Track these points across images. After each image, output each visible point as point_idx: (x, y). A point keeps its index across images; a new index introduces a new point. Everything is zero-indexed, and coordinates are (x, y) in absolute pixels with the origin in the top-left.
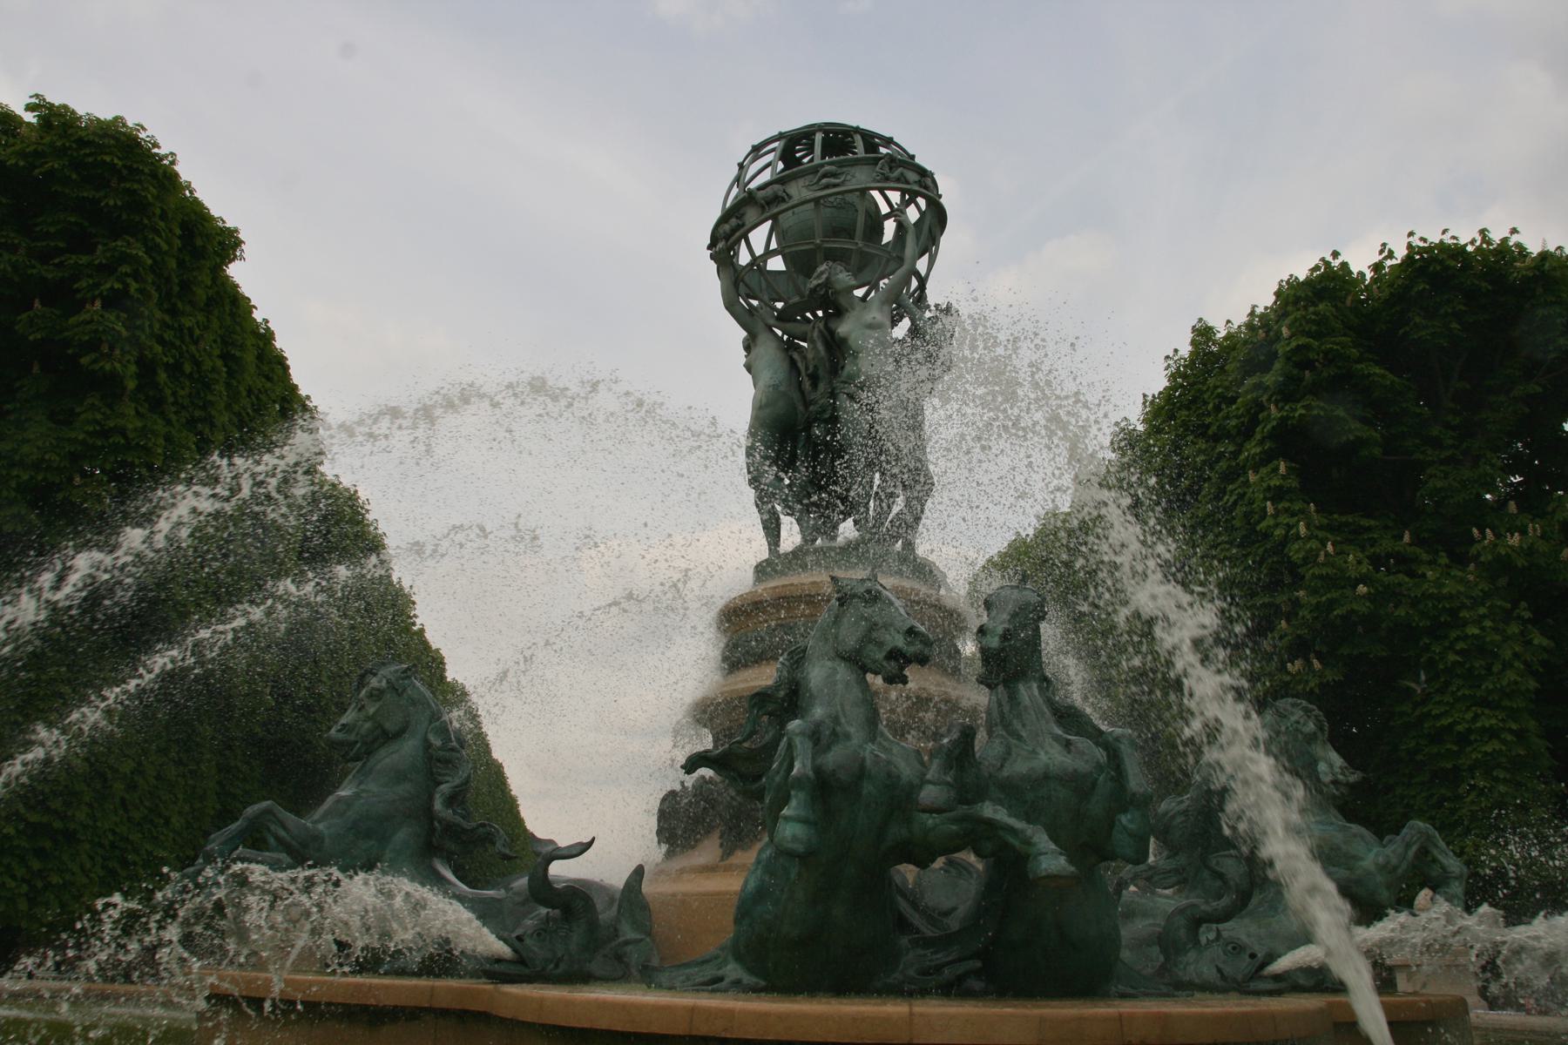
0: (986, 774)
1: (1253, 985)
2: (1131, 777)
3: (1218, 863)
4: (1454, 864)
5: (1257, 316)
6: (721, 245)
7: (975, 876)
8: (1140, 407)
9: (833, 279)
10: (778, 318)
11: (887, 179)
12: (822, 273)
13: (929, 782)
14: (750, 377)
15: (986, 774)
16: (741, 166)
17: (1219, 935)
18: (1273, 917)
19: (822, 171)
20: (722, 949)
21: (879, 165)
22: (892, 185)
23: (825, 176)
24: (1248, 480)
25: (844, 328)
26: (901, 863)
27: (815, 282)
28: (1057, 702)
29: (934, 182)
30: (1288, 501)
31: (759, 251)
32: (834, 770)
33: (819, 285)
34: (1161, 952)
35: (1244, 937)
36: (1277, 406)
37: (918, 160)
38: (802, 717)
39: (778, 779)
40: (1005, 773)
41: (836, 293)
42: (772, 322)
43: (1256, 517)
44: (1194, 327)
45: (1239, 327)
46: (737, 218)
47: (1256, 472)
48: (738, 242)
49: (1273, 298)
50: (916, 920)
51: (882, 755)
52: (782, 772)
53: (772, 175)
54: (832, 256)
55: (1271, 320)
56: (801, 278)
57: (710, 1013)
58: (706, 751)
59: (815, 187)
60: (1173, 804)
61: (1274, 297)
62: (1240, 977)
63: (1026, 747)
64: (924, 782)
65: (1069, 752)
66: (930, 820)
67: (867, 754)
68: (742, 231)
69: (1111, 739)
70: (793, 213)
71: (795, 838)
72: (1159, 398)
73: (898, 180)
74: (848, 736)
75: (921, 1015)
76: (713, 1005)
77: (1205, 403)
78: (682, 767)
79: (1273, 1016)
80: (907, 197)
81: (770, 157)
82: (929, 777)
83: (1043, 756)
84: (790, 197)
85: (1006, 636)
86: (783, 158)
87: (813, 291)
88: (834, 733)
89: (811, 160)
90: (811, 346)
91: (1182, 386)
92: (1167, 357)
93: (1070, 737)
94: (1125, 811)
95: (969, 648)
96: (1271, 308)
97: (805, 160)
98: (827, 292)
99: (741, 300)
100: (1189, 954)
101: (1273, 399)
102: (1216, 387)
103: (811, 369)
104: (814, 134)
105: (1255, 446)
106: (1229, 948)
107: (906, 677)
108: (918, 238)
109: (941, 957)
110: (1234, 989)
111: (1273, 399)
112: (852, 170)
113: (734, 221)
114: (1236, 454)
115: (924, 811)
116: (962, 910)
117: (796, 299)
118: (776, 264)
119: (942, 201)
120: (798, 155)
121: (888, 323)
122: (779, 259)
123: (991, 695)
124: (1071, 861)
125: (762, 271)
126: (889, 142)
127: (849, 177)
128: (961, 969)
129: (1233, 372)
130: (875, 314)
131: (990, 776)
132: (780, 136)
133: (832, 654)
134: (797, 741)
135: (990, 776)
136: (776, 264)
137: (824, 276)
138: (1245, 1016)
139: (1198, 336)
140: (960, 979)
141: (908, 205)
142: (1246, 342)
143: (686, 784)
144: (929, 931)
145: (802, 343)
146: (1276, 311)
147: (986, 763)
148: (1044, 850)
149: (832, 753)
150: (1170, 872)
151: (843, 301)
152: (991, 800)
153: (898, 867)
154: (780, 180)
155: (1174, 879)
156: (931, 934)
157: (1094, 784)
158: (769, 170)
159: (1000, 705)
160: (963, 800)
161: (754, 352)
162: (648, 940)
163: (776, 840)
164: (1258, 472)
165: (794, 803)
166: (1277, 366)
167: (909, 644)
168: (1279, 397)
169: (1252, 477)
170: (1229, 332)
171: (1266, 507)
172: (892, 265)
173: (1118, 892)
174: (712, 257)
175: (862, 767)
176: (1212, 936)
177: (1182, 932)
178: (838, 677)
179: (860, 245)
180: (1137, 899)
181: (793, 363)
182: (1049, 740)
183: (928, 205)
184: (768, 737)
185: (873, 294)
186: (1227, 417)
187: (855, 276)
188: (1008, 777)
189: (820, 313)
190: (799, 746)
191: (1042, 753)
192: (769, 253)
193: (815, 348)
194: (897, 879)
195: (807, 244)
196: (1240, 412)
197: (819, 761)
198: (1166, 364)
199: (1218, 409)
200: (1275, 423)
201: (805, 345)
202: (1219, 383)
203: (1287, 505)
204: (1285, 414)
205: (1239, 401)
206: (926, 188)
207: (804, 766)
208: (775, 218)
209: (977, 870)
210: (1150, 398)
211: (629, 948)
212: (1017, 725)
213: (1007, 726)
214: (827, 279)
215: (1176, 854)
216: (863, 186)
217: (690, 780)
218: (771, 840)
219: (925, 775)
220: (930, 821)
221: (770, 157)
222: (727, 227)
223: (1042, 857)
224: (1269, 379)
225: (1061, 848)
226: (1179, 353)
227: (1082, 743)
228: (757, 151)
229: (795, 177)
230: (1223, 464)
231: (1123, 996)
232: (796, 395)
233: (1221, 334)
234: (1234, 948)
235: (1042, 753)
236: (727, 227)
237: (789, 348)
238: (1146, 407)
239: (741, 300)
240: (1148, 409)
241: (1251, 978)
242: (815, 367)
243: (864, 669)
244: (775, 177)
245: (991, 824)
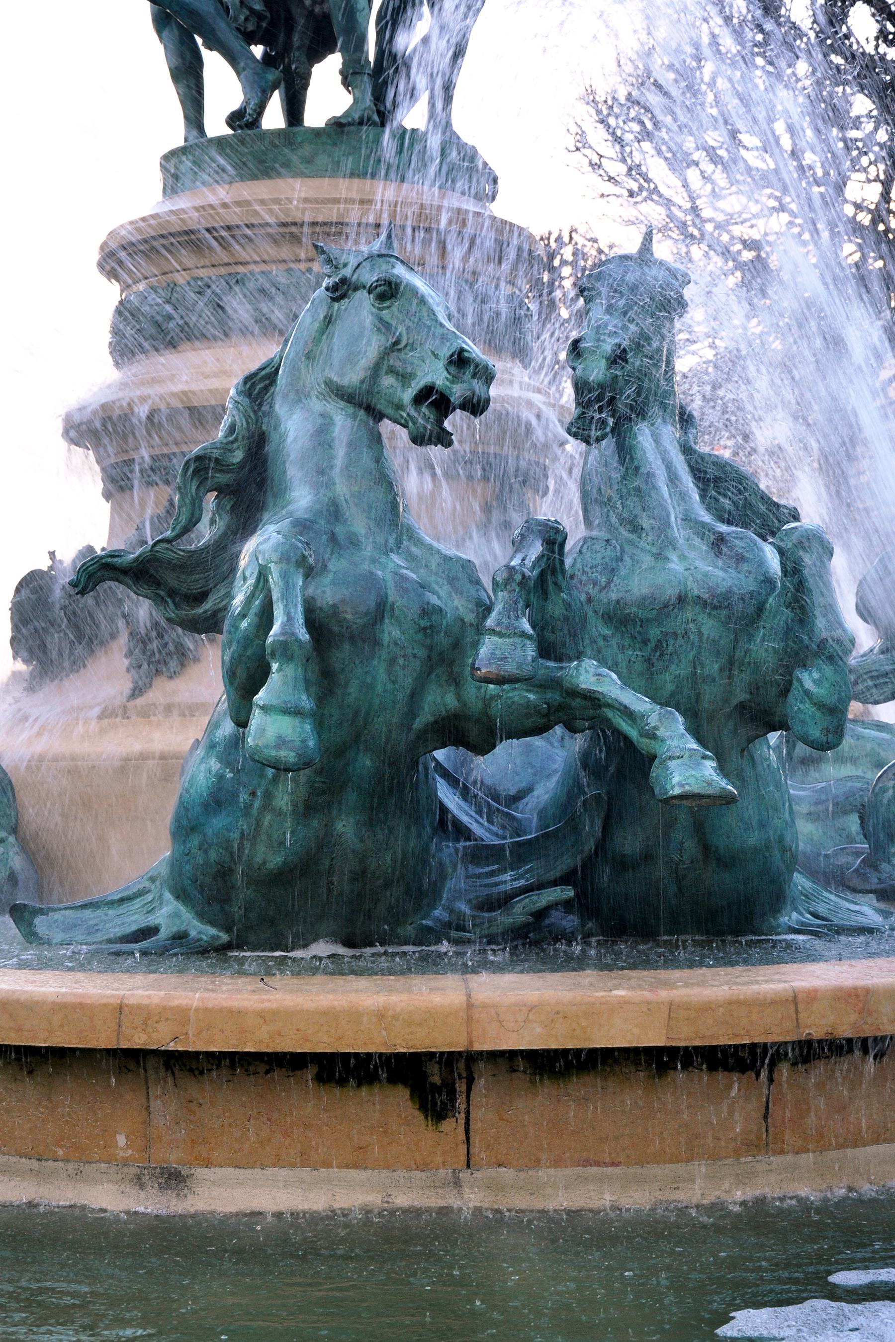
65: (719, 553)
71: (281, 742)
83: (675, 565)
109: (508, 880)
124: (722, 769)
131: (589, 600)
143: (58, 556)
165: (275, 678)
167: (455, 379)
188: (618, 602)
191: (674, 558)
197: (310, 591)
223: (672, 764)
235: (674, 558)
243: (379, 416)
245: (593, 700)
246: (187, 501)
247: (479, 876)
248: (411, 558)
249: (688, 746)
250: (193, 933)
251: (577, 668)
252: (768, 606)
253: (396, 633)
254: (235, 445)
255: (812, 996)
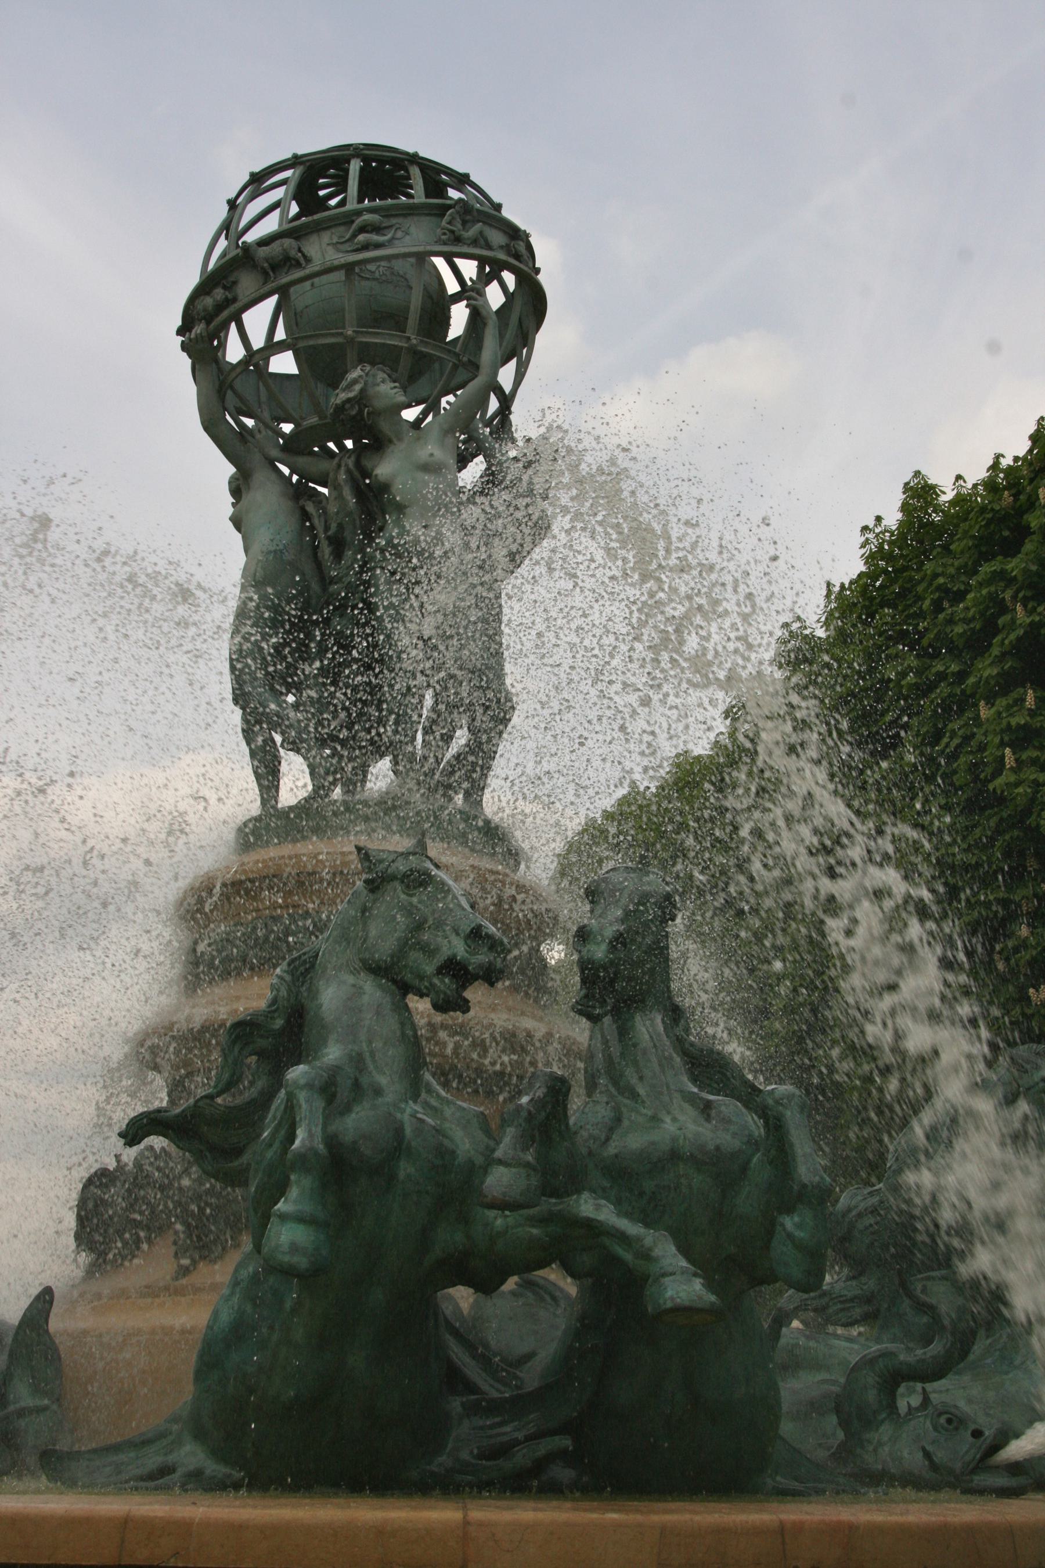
0: (584, 1151)
1: (981, 1479)
2: (800, 1159)
3: (924, 1290)
4: (996, 1001)
5: (1002, 471)
6: (198, 329)
7: (562, 1304)
8: (822, 602)
9: (371, 391)
10: (285, 449)
11: (458, 240)
12: (355, 382)
13: (500, 1162)
14: (239, 536)
15: (584, 1151)
16: (232, 204)
17: (926, 1400)
18: (1007, 1373)
19: (359, 221)
20: (175, 1419)
21: (447, 218)
22: (465, 249)
23: (362, 229)
24: (978, 715)
25: (384, 469)
26: (454, 1285)
27: (343, 396)
28: (692, 1044)
29: (530, 248)
30: (1035, 747)
31: (258, 342)
32: (355, 1142)
33: (349, 400)
34: (840, 1424)
35: (962, 1404)
36: (1025, 606)
37: (506, 213)
38: (309, 1063)
39: (269, 1154)
40: (612, 1149)
41: (375, 413)
42: (275, 453)
43: (989, 770)
44: (907, 484)
45: (975, 486)
46: (225, 288)
47: (990, 703)
48: (225, 327)
49: (1028, 444)
50: (472, 1370)
51: (429, 1120)
52: (277, 1145)
53: (280, 224)
54: (368, 355)
55: (1023, 477)
56: (320, 389)
57: (151, 1528)
58: (159, 1111)
59: (347, 247)
60: (860, 1198)
61: (1029, 443)
62: (958, 1466)
63: (645, 1111)
64: (490, 1162)
65: (708, 1119)
66: (499, 1221)
67: (406, 1118)
68: (232, 308)
69: (770, 1102)
70: (312, 285)
71: (294, 1248)
72: (850, 589)
73: (475, 242)
74: (378, 1092)
75: (481, 1524)
76: (160, 1514)
77: (919, 598)
78: (121, 1135)
79: (1010, 1532)
80: (488, 269)
81: (278, 193)
82: (498, 1154)
83: (669, 1126)
84: (308, 260)
85: (619, 941)
86: (298, 197)
87: (340, 409)
88: (357, 1085)
89: (342, 203)
90: (335, 494)
91: (885, 571)
92: (865, 529)
93: (711, 1097)
94: (789, 1210)
95: (555, 953)
96: (1024, 458)
97: (333, 202)
98: (361, 412)
99: (228, 417)
100: (882, 1429)
101: (1021, 595)
102: (936, 576)
103: (334, 527)
104: (349, 163)
105: (990, 665)
106: (942, 1420)
107: (467, 1001)
108: (501, 336)
109: (510, 1431)
110: (953, 1486)
111: (1021, 595)
112: (406, 222)
113: (219, 293)
114: (961, 676)
115: (492, 1206)
116: (547, 1353)
117: (314, 420)
118: (284, 364)
119: (541, 278)
120: (321, 193)
121: (452, 462)
122: (289, 355)
123: (592, 1031)
124: (709, 1285)
125: (262, 371)
126: (462, 180)
127: (399, 234)
128: (544, 1447)
129: (962, 552)
130: (432, 449)
131: (590, 1153)
132: (295, 161)
133: (358, 965)
134: (302, 1096)
135: (590, 1153)
136: (284, 364)
137: (357, 387)
138: (970, 1531)
139: (912, 498)
140: (539, 1467)
141: (488, 283)
142: (983, 509)
144: (493, 1391)
145: (320, 489)
146: (1031, 464)
147: (585, 1134)
148: (670, 1269)
149: (353, 1115)
150: (852, 1300)
151: (385, 426)
152: (593, 1191)
153: (451, 1291)
154: (291, 232)
155: (858, 1312)
156: (495, 1394)
157: (744, 1168)
158: (276, 213)
159: (606, 1042)
160: (549, 1190)
161: (246, 499)
162: (55, 1407)
163: (265, 1250)
164: (993, 705)
165: (294, 1192)
166: (1028, 546)
168: (1029, 594)
169: (985, 712)
170: (958, 494)
171: (1003, 756)
172: (462, 375)
173: (775, 1335)
174: (184, 347)
175: (399, 1131)
176: (915, 1401)
177: (871, 1396)
178: (366, 999)
179: (414, 342)
180: (802, 1342)
181: (305, 516)
182: (677, 1099)
183: (518, 283)
184: (251, 1094)
185: (430, 418)
186: (950, 621)
187: (404, 388)
188: (616, 1156)
189: (349, 444)
190: (304, 1106)
191: (668, 1119)
192: (272, 347)
193: (340, 497)
194: (447, 1309)
195: (333, 335)
196: (971, 614)
197: (332, 1128)
198: (863, 539)
199: (938, 608)
200: (1021, 632)
201: (325, 491)
202: (940, 570)
203: (1035, 754)
204: (1037, 619)
205: (969, 597)
206: (517, 256)
207: (311, 1135)
208: (283, 292)
209: (568, 1296)
210: (837, 589)
211: (22, 1423)
212: (631, 1075)
213: (616, 1079)
214: (362, 391)
215: (861, 1274)
216: (421, 249)
217: (130, 1155)
218: (258, 1248)
219: (493, 1150)
220: (499, 1222)
221: (278, 193)
222: (208, 301)
223: (667, 1280)
224: (1014, 566)
225: (694, 1265)
226: (884, 523)
227: (726, 1105)
228: (257, 182)
229: (318, 228)
230: (943, 690)
231: (784, 1494)
232: (308, 567)
233: (948, 496)
234: (949, 1421)
235: (668, 1119)
236: (208, 301)
237: (300, 494)
238: (830, 602)
239: (228, 417)
240: (833, 605)
241: (977, 1467)
242: (341, 527)
243: (405, 989)
244: (286, 226)
245: (591, 1227)
246: (230, 1061)
247: (482, 1428)
248: (426, 1105)
249: (680, 1264)
250: (208, 1472)
251: (577, 1201)
252: (752, 1165)
253: (411, 1170)
254: (276, 1015)
255: (799, 1528)
